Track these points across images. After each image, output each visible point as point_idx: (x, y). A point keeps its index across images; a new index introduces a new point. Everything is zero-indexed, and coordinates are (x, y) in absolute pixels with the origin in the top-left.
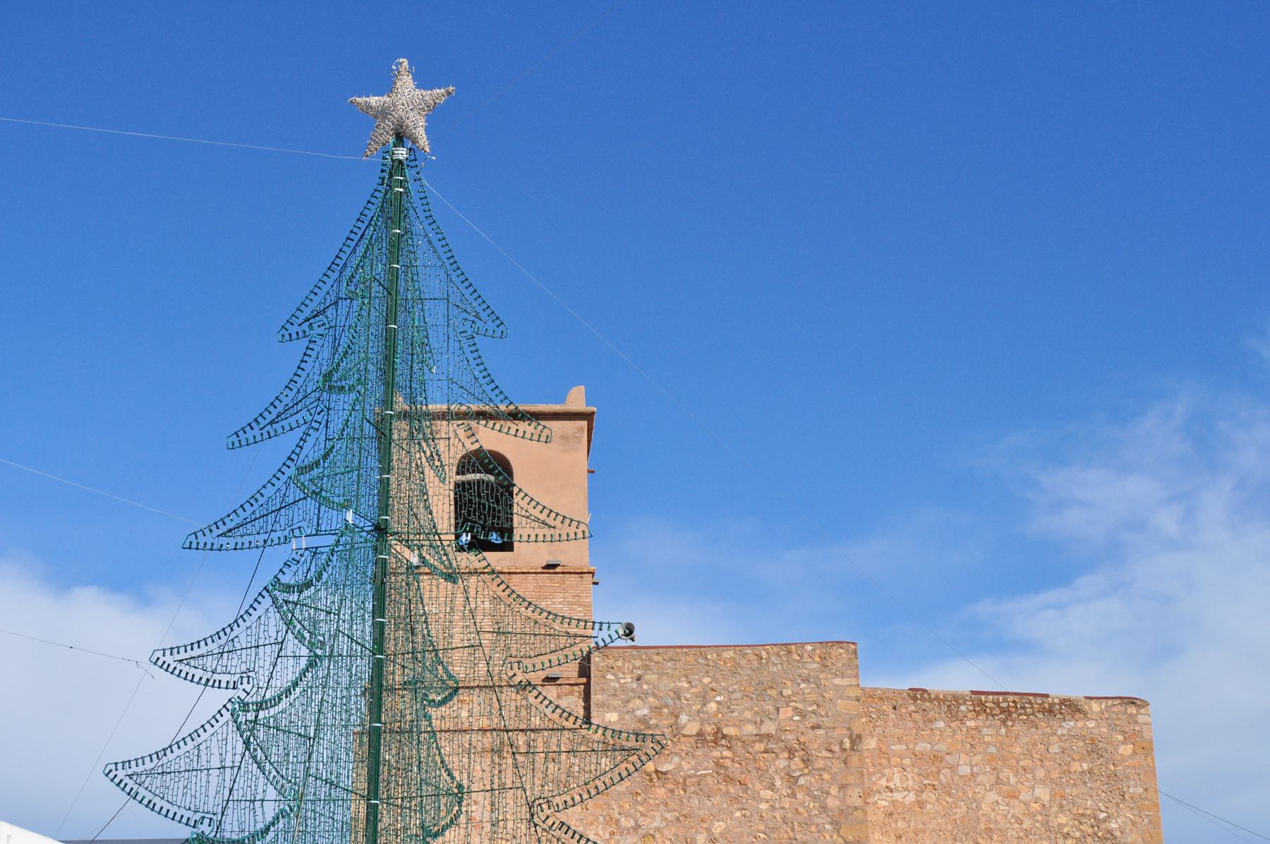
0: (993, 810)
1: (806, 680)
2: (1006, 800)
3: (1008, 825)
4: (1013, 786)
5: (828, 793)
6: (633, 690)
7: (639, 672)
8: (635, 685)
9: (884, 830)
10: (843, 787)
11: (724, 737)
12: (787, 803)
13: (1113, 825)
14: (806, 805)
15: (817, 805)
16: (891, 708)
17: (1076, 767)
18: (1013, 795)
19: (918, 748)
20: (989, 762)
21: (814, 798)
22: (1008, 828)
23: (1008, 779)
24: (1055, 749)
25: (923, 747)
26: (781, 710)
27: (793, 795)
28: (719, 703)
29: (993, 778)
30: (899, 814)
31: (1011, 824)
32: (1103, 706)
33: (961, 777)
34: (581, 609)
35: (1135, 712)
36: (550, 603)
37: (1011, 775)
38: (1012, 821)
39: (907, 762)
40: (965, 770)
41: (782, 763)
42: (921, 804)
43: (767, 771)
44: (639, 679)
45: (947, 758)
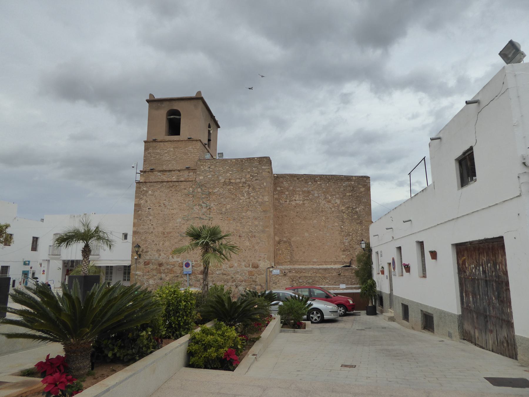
1: (254, 167)
3: (328, 210)
5: (259, 198)
6: (207, 171)
7: (209, 166)
8: (208, 169)
9: (293, 211)
11: (231, 183)
12: (248, 200)
13: (357, 210)
15: (256, 201)
16: (297, 179)
17: (348, 194)
19: (304, 189)
20: (323, 193)
21: (255, 199)
22: (327, 210)
23: (328, 197)
25: (305, 189)
27: (249, 198)
28: (230, 173)
29: (324, 197)
30: (298, 206)
32: (357, 178)
33: (315, 197)
35: (366, 179)
37: (329, 196)
39: (301, 193)
40: (316, 195)
41: (246, 189)
42: (304, 204)
43: (242, 192)
44: (209, 168)
45: (312, 192)
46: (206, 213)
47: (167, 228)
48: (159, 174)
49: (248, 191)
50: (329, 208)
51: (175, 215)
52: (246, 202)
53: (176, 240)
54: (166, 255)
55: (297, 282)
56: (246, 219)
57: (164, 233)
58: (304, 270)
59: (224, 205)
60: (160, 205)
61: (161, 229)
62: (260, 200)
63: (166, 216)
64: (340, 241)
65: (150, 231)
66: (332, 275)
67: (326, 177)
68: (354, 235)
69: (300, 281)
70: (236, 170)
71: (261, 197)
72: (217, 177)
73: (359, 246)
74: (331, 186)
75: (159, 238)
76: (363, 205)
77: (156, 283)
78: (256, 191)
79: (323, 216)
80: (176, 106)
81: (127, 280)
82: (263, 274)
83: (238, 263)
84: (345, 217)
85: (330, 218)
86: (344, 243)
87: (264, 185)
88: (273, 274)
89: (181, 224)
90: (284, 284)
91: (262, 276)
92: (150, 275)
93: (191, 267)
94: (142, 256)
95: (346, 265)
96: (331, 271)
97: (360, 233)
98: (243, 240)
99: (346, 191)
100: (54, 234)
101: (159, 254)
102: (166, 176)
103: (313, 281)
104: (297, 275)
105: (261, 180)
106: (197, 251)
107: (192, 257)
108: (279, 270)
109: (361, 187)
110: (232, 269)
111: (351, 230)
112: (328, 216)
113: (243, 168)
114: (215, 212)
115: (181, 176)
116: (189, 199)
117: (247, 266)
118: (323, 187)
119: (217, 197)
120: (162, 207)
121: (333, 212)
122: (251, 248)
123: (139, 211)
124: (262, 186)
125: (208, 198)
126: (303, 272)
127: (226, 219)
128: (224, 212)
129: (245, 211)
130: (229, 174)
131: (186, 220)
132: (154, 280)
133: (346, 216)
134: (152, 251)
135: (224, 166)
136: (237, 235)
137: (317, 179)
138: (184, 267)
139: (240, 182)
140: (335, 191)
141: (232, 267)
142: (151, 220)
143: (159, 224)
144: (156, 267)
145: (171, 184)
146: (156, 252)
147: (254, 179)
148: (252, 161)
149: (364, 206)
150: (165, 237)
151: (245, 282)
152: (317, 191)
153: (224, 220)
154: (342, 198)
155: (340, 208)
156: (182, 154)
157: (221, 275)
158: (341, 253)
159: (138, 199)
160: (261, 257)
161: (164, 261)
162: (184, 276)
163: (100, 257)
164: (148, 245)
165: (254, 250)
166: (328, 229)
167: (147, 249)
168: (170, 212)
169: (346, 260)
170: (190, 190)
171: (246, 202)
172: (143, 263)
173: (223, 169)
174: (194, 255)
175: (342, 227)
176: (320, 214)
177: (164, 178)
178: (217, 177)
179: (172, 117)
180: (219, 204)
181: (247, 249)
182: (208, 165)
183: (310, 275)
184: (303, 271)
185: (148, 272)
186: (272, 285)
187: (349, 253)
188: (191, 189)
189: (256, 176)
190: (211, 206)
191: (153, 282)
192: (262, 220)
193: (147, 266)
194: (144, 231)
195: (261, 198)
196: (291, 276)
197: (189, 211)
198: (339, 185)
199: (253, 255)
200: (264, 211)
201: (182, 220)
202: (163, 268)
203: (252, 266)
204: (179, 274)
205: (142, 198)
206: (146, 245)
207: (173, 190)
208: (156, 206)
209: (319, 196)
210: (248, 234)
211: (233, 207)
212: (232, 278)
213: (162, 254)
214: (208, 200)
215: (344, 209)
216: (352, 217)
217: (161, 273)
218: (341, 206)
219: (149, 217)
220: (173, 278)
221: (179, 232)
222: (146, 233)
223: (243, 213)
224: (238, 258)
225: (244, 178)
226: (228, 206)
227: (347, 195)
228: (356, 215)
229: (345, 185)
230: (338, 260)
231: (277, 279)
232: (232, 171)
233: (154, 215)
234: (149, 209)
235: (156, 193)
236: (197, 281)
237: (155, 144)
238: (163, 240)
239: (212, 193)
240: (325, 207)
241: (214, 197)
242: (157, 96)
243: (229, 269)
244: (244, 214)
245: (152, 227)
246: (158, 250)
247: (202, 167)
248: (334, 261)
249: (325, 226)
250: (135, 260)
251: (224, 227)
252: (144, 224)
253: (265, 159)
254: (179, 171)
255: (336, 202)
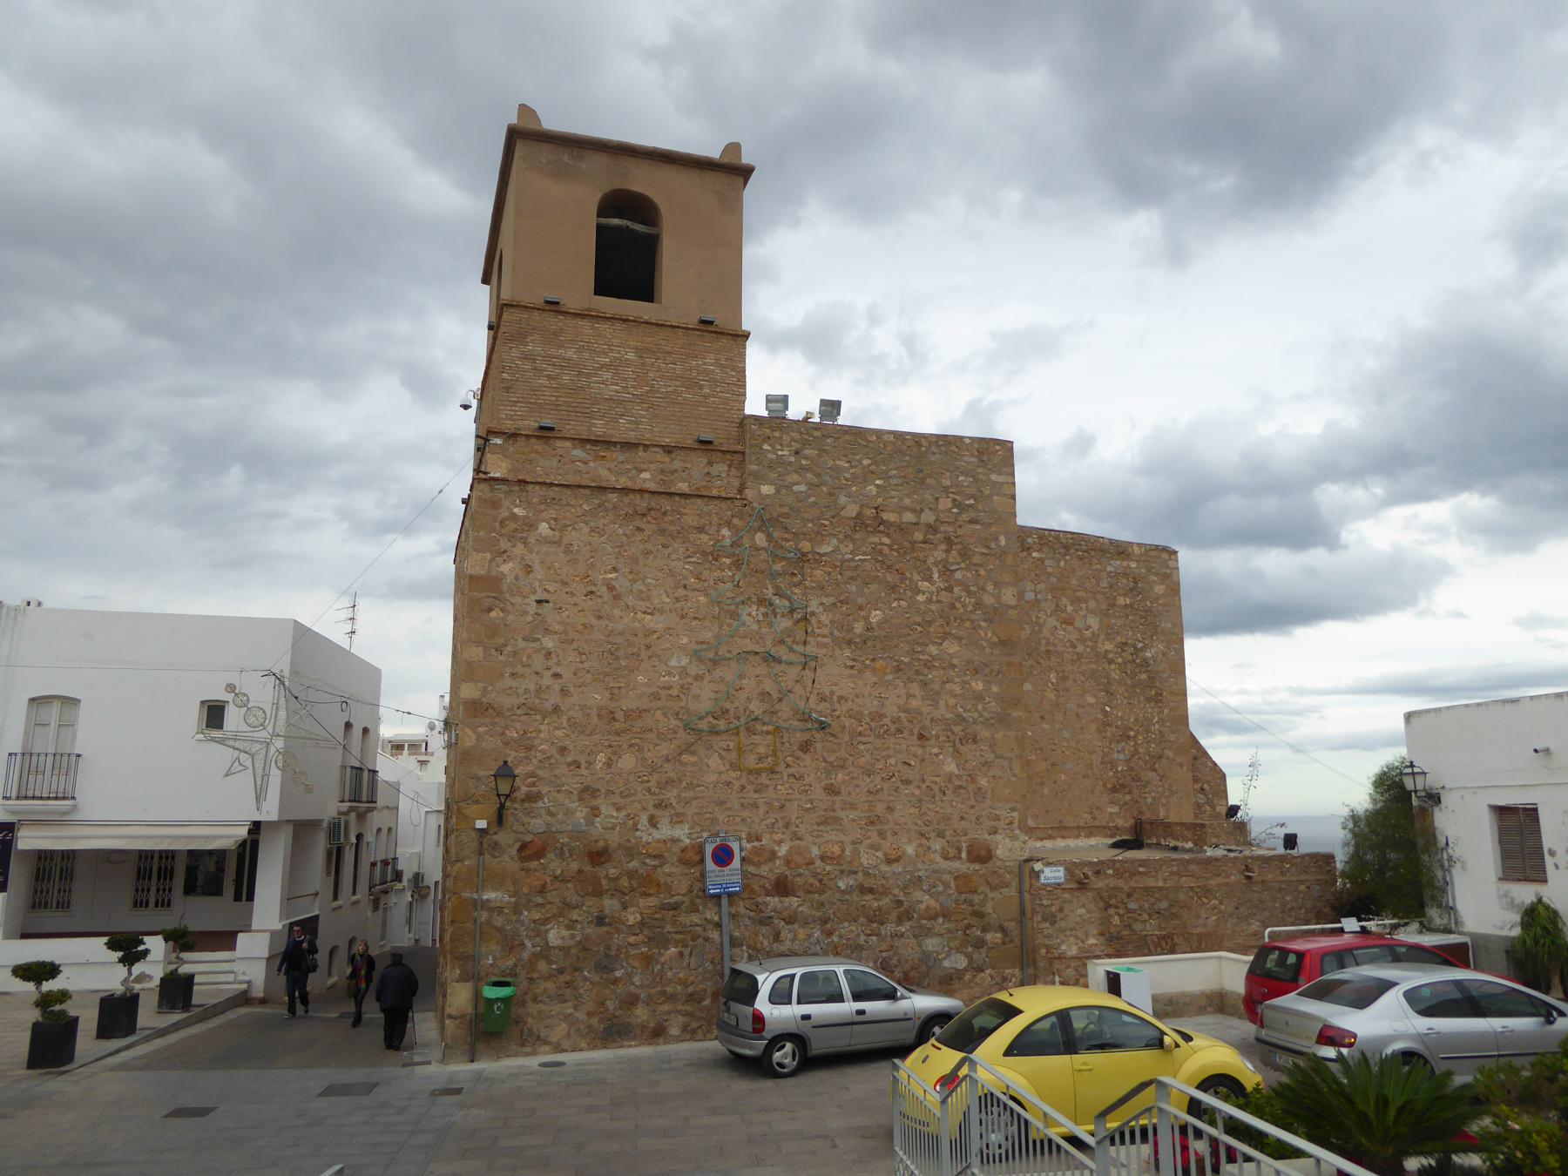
0: (1052, 634)
2: (1064, 626)
4: (1069, 614)
6: (790, 464)
8: (792, 459)
10: (997, 585)
11: (883, 522)
12: (944, 596)
13: (1148, 654)
14: (962, 600)
15: (973, 600)
17: (1121, 601)
18: (1068, 622)
21: (969, 593)
22: (1064, 652)
23: (1066, 607)
24: (1104, 584)
26: (940, 500)
27: (949, 589)
28: (877, 486)
29: (1053, 606)
31: (1066, 647)
32: (1143, 550)
33: (1027, 602)
34: (734, 374)
35: (1167, 558)
36: (700, 363)
37: (1068, 603)
38: (1068, 645)
41: (939, 554)
43: (925, 562)
44: (797, 453)
46: (789, 636)
47: (623, 690)
48: (578, 453)
49: (945, 562)
50: (1068, 645)
51: (658, 638)
52: (938, 601)
53: (666, 749)
54: (624, 813)
55: (1121, 912)
56: (942, 672)
57: (612, 712)
58: (1144, 867)
59: (861, 608)
60: (594, 589)
61: (597, 697)
62: (988, 600)
63: (619, 640)
64: (1103, 758)
65: (548, 706)
66: (1226, 880)
67: (1057, 538)
68: (1141, 738)
69: (1132, 906)
70: (900, 477)
71: (990, 588)
72: (831, 494)
73: (1154, 774)
74: (1074, 570)
75: (591, 734)
76: (1162, 641)
77: (578, 939)
78: (974, 565)
79: (1051, 668)
80: (642, 181)
81: (152, 904)
82: (1006, 887)
83: (918, 842)
84: (1115, 675)
85: (1071, 679)
86: (1113, 764)
87: (1000, 546)
88: (1043, 884)
89: (689, 680)
90: (1078, 920)
91: (1005, 891)
92: (548, 907)
93: (736, 863)
94: (511, 818)
95: (1121, 838)
96: (1223, 868)
97: (1157, 732)
98: (936, 750)
99: (1115, 591)
100: (32, 700)
101: (592, 808)
102: (612, 465)
103: (1172, 906)
104: (1121, 883)
105: (990, 524)
106: (757, 796)
107: (738, 819)
108: (1061, 869)
109: (1154, 582)
110: (898, 868)
111: (1132, 720)
112: (1066, 669)
113: (922, 471)
114: (824, 636)
115: (676, 475)
116: (718, 574)
117: (951, 855)
118: (1049, 570)
119: (829, 574)
120: (599, 601)
121: (1080, 656)
122: (964, 785)
123: (490, 610)
124: (993, 545)
125: (793, 574)
126: (1140, 873)
127: (867, 667)
128: (861, 636)
129: (938, 638)
130: (872, 489)
131: (710, 660)
132: (568, 928)
133: (1118, 672)
134: (556, 795)
135: (853, 454)
136: (911, 730)
137: (1030, 540)
138: (710, 864)
139: (915, 524)
140: (1086, 588)
141: (897, 860)
142: (550, 653)
143: (589, 672)
144: (575, 866)
145: (642, 503)
146: (575, 797)
147: (965, 517)
148: (953, 448)
149: (1164, 645)
150: (618, 734)
151: (944, 917)
152: (1033, 582)
153: (860, 671)
154: (1104, 614)
155: (1099, 645)
156: (678, 383)
157: (854, 895)
158: (1106, 798)
159: (488, 556)
160: (997, 818)
161: (614, 839)
162: (705, 906)
163: (75, 806)
164: (540, 768)
165: (975, 793)
166: (1065, 714)
167: (533, 784)
168: (637, 624)
169: (1120, 822)
170: (724, 537)
171: (938, 601)
172: (514, 852)
173: (852, 467)
174: (745, 814)
175: (1108, 709)
176: (1041, 661)
177: (604, 473)
178: (831, 494)
179: (616, 221)
180: (839, 605)
181: (950, 786)
182: (792, 440)
183: (1161, 884)
184: (1141, 869)
185: (540, 892)
186: (1041, 926)
187: (1128, 797)
188: (725, 532)
189: (970, 506)
190: (809, 610)
191: (562, 938)
192: (997, 675)
193: (534, 864)
194: (516, 701)
195: (992, 594)
196: (1102, 888)
197: (721, 626)
198: (1097, 570)
199: (972, 811)
200: (1002, 643)
201: (690, 662)
202: (613, 871)
203: (969, 853)
204: (685, 895)
205: (505, 552)
206: (531, 768)
207: (650, 528)
208: (573, 594)
209: (1037, 601)
210: (953, 728)
211: (894, 621)
212: (899, 903)
213: (606, 810)
214: (796, 585)
215: (1112, 651)
216: (1133, 678)
217: (599, 893)
218: (1103, 640)
219: (539, 640)
220: (657, 916)
221: (677, 714)
222: (530, 710)
223: (930, 646)
224: (919, 822)
225: (931, 509)
226: (876, 616)
227: (1118, 603)
228: (1144, 673)
229: (1113, 569)
230: (1097, 823)
231: (1055, 902)
232: (885, 476)
233: (566, 632)
234: (539, 602)
235: (572, 536)
236: (762, 923)
237: (552, 321)
238: (610, 746)
239: (810, 556)
240: (1056, 638)
241: (818, 573)
242: (552, 122)
243: (884, 868)
244: (933, 649)
245: (557, 688)
246: (588, 792)
247: (766, 447)
248: (1086, 823)
249: (1057, 705)
250: (474, 835)
251: (863, 696)
252: (519, 669)
253: (998, 447)
254: (668, 450)
255: (1087, 624)
